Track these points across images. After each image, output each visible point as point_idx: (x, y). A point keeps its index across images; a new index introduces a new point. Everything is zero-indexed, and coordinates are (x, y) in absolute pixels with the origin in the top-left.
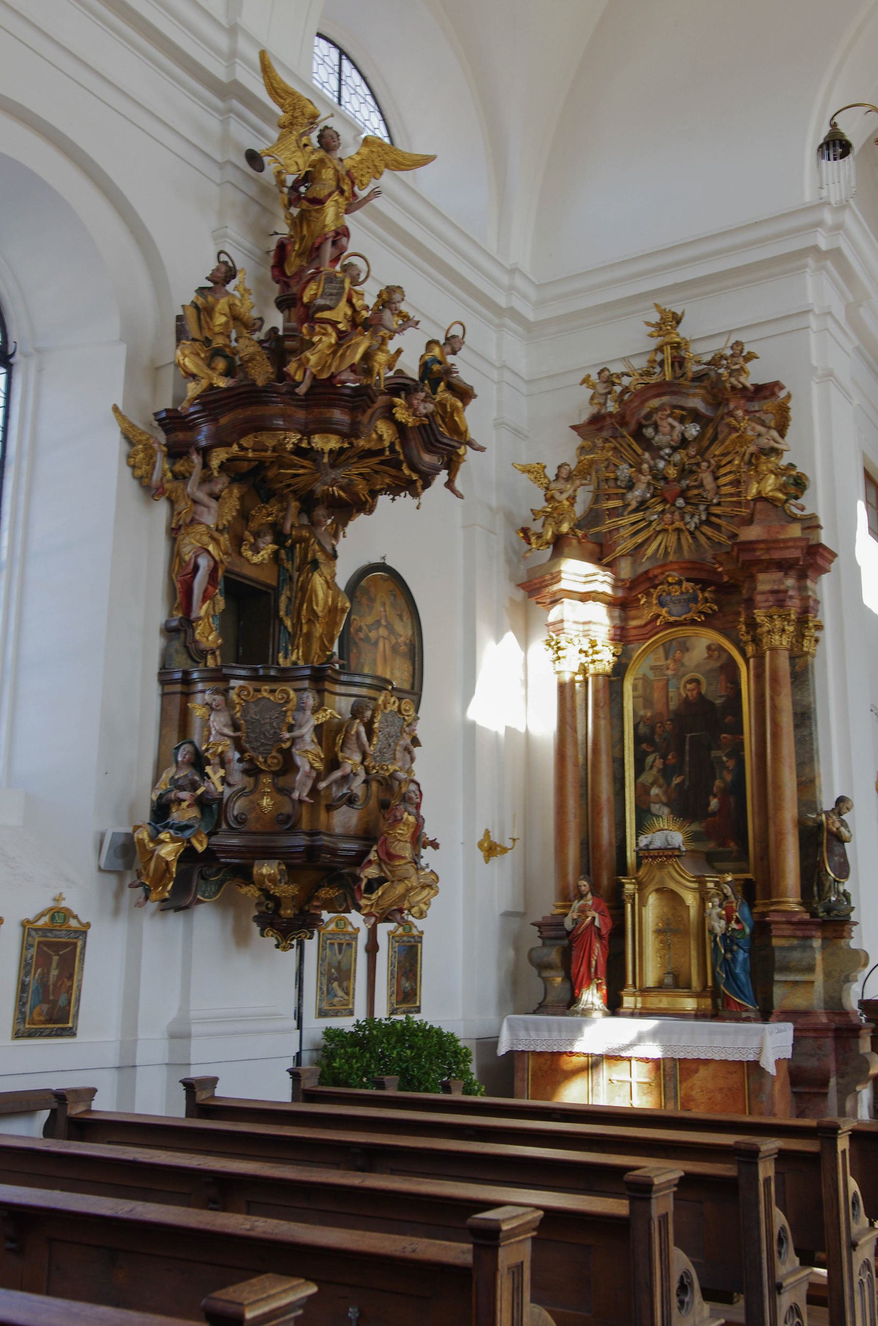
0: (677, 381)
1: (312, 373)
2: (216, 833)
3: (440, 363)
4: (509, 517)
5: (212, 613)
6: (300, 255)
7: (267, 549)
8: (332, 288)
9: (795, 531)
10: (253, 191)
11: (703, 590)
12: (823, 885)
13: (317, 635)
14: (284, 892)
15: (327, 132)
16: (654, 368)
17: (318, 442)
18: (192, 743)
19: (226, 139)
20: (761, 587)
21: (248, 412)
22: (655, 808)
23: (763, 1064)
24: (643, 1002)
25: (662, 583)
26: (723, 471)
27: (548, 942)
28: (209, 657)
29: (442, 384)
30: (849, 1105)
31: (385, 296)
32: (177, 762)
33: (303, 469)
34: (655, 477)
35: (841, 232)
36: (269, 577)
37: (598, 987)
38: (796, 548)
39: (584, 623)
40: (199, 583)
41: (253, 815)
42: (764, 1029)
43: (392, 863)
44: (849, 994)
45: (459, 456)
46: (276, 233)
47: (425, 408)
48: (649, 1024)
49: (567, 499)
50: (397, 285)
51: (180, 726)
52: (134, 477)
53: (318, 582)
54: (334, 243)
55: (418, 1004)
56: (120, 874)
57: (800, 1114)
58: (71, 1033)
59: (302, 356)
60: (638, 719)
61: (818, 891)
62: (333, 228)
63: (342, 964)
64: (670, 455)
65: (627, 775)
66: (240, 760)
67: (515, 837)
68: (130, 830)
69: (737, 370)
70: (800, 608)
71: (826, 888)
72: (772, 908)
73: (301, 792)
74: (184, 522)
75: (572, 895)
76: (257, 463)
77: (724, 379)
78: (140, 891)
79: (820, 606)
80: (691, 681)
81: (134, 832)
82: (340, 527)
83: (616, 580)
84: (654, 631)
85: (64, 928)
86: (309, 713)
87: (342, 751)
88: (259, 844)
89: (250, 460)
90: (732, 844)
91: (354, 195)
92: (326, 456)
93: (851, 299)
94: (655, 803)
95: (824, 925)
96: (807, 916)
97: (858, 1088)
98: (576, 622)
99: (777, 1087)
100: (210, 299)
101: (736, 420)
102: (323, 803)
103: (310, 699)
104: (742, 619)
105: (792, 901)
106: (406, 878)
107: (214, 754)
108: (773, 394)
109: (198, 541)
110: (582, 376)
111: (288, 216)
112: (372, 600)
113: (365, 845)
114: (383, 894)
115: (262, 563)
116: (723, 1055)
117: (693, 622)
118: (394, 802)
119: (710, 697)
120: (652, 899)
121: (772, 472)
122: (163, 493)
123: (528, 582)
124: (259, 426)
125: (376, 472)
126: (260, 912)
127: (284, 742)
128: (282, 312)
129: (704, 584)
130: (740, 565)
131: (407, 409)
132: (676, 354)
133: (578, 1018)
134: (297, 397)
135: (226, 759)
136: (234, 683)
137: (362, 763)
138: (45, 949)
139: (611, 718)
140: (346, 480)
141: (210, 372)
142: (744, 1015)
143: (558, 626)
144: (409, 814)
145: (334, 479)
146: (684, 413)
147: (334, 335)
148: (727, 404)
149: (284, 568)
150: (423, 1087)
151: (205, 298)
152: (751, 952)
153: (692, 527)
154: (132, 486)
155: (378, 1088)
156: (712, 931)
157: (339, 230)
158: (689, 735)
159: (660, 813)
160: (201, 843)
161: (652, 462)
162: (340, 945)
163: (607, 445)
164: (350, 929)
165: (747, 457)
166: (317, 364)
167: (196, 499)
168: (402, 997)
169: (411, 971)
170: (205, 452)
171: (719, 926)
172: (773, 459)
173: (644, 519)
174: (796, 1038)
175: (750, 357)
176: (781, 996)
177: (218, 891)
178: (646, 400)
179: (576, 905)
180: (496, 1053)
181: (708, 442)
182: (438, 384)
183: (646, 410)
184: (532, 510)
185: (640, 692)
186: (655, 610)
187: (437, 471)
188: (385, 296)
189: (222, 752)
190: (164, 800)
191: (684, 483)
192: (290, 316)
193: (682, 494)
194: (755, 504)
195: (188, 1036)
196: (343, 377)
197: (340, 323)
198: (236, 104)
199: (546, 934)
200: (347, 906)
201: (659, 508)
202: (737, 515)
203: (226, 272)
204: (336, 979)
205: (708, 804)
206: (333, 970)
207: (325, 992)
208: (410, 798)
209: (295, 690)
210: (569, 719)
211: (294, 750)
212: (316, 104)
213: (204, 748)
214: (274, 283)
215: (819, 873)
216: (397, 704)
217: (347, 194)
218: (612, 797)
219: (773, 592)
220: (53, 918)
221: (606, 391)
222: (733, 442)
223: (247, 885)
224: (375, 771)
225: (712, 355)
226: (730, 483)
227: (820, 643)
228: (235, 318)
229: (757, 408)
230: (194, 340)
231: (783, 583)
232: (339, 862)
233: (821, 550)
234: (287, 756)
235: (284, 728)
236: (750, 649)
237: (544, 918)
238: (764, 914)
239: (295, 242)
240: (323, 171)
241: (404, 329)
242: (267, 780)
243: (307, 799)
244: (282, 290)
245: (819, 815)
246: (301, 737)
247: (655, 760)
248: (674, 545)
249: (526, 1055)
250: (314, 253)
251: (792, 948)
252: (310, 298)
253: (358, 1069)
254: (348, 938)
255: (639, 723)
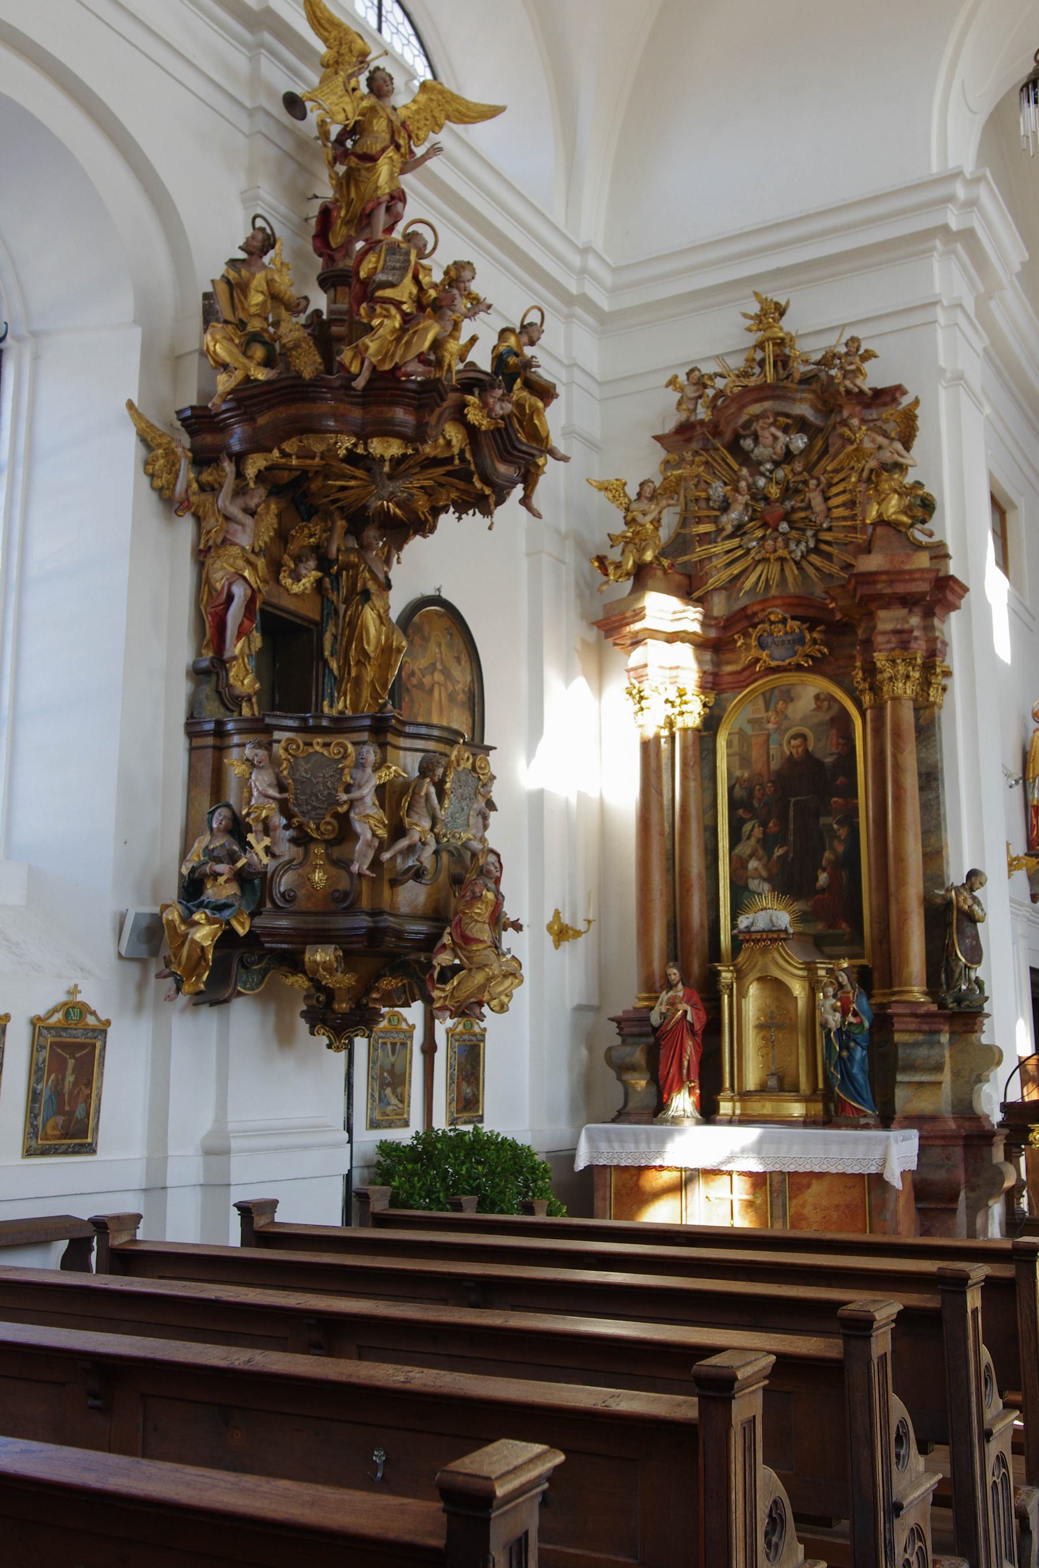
0: (781, 384)
1: (371, 363)
2: (260, 913)
3: (517, 355)
4: (580, 544)
5: (247, 651)
6: (347, 223)
7: (310, 577)
8: (396, 261)
9: (923, 560)
10: (288, 144)
11: (811, 630)
12: (953, 972)
13: (369, 680)
14: (338, 983)
15: (378, 74)
16: (752, 368)
17: (377, 447)
18: (228, 806)
19: (255, 80)
20: (881, 627)
21: (293, 410)
22: (753, 884)
23: (887, 1177)
24: (742, 1108)
25: (762, 622)
26: (834, 490)
27: (629, 1040)
28: (244, 704)
29: (519, 380)
30: (979, 1222)
31: (453, 273)
32: (211, 829)
33: (354, 481)
34: (753, 497)
35: (975, 209)
36: (311, 610)
37: (691, 1091)
38: (924, 580)
39: (671, 668)
40: (234, 615)
41: (303, 891)
42: (888, 1138)
43: (469, 948)
44: (979, 1097)
45: (538, 467)
46: (316, 197)
47: (502, 408)
48: (751, 1134)
49: (651, 522)
50: (466, 260)
51: (212, 787)
52: (153, 488)
53: (369, 617)
54: (388, 209)
55: (406, 1116)
56: (143, 962)
57: (925, 1233)
58: (90, 1149)
59: (360, 342)
60: (733, 782)
61: (947, 978)
62: (387, 191)
63: (396, 1067)
64: (771, 472)
65: (720, 845)
66: (286, 827)
67: (591, 918)
68: (157, 910)
69: (852, 371)
70: (927, 651)
71: (957, 975)
72: (894, 999)
73: (361, 865)
74: (215, 542)
75: (658, 985)
76: (299, 472)
77: (837, 381)
78: (170, 980)
79: (948, 649)
80: (795, 737)
81: (162, 912)
82: (394, 551)
83: (706, 616)
84: (753, 677)
85: (80, 1026)
86: (369, 770)
87: (408, 816)
88: (311, 926)
89: (290, 469)
90: (844, 925)
91: (411, 152)
92: (387, 464)
93: (982, 289)
94: (753, 878)
95: (952, 1018)
96: (934, 1008)
97: (990, 1203)
98: (661, 667)
99: (902, 1202)
100: (244, 273)
101: (850, 430)
102: (387, 877)
103: (371, 754)
104: (858, 664)
105: (917, 992)
106: (486, 965)
107: (257, 819)
108: (895, 400)
109: (232, 566)
110: (668, 376)
111: (333, 176)
112: (426, 640)
113: (436, 927)
114: (459, 983)
115: (303, 593)
116: (840, 1167)
117: (799, 668)
118: (471, 876)
119: (818, 755)
120: (753, 989)
121: (895, 491)
122: (188, 508)
123: (605, 619)
124: (305, 428)
125: (441, 485)
126: (308, 1006)
127: (341, 805)
128: (326, 292)
129: (812, 623)
130: (857, 600)
131: (481, 409)
132: (779, 352)
133: (667, 1127)
134: (353, 392)
135: (271, 826)
136: (277, 735)
137: (432, 830)
138: (59, 1051)
139: (702, 778)
140: (405, 495)
141: (246, 361)
142: (863, 1121)
143: (639, 672)
144: (488, 890)
145: (392, 493)
146: (789, 421)
147: (398, 317)
148: (841, 412)
149: (328, 599)
150: (498, 1209)
151: (239, 272)
152: (870, 1049)
153: (798, 555)
154: (150, 498)
155: (454, 1210)
156: (824, 1025)
157: (395, 194)
158: (793, 800)
159: (760, 890)
160: (242, 924)
161: (750, 480)
162: (394, 1045)
163: (697, 459)
164: (404, 1026)
165: (865, 474)
166: (378, 352)
167: (228, 515)
168: (462, 1104)
169: (473, 1074)
170: (239, 459)
171: (834, 1020)
172: (896, 476)
173: (740, 546)
174: (922, 1148)
175: (868, 356)
176: (904, 1100)
177: (261, 982)
178: (745, 406)
179: (664, 996)
180: (573, 1168)
181: (816, 457)
182: (514, 381)
183: (744, 418)
184: (609, 535)
185: (736, 748)
186: (754, 653)
187: (514, 484)
188: (453, 273)
189: (267, 817)
190: (197, 875)
191: (788, 505)
192: (335, 296)
193: (786, 517)
194: (874, 529)
195: (226, 1152)
196: (410, 368)
197: (405, 303)
198: (268, 37)
199: (627, 1031)
200: (407, 999)
201: (759, 533)
202: (851, 542)
203: (264, 240)
204: (389, 1085)
205: (816, 879)
206: (386, 1074)
207: (378, 1099)
208: (489, 872)
209: (354, 744)
210: (653, 780)
211: (352, 815)
212: (366, 40)
213: (244, 812)
214: (316, 256)
215: (947, 958)
216: (471, 761)
217: (403, 150)
218: (703, 871)
219: (896, 632)
220: (67, 1014)
221: (697, 394)
222: (849, 456)
223: (293, 974)
224: (445, 839)
225: (824, 353)
226: (844, 505)
227: (948, 692)
228: (275, 297)
229: (875, 417)
230: (226, 322)
231: (908, 622)
232: (407, 947)
233: (951, 583)
234: (344, 820)
235: (341, 789)
236: (867, 699)
237: (624, 1012)
238: (883, 1006)
239: (340, 208)
240: (375, 121)
241: (475, 314)
242: (319, 850)
243: (368, 873)
244: (326, 265)
245: (948, 890)
246: (361, 799)
247: (752, 829)
248: (777, 577)
249: (608, 1170)
250: (363, 220)
251: (916, 1045)
252: (368, 273)
253: (420, 1188)
254: (402, 1036)
255: (734, 785)
